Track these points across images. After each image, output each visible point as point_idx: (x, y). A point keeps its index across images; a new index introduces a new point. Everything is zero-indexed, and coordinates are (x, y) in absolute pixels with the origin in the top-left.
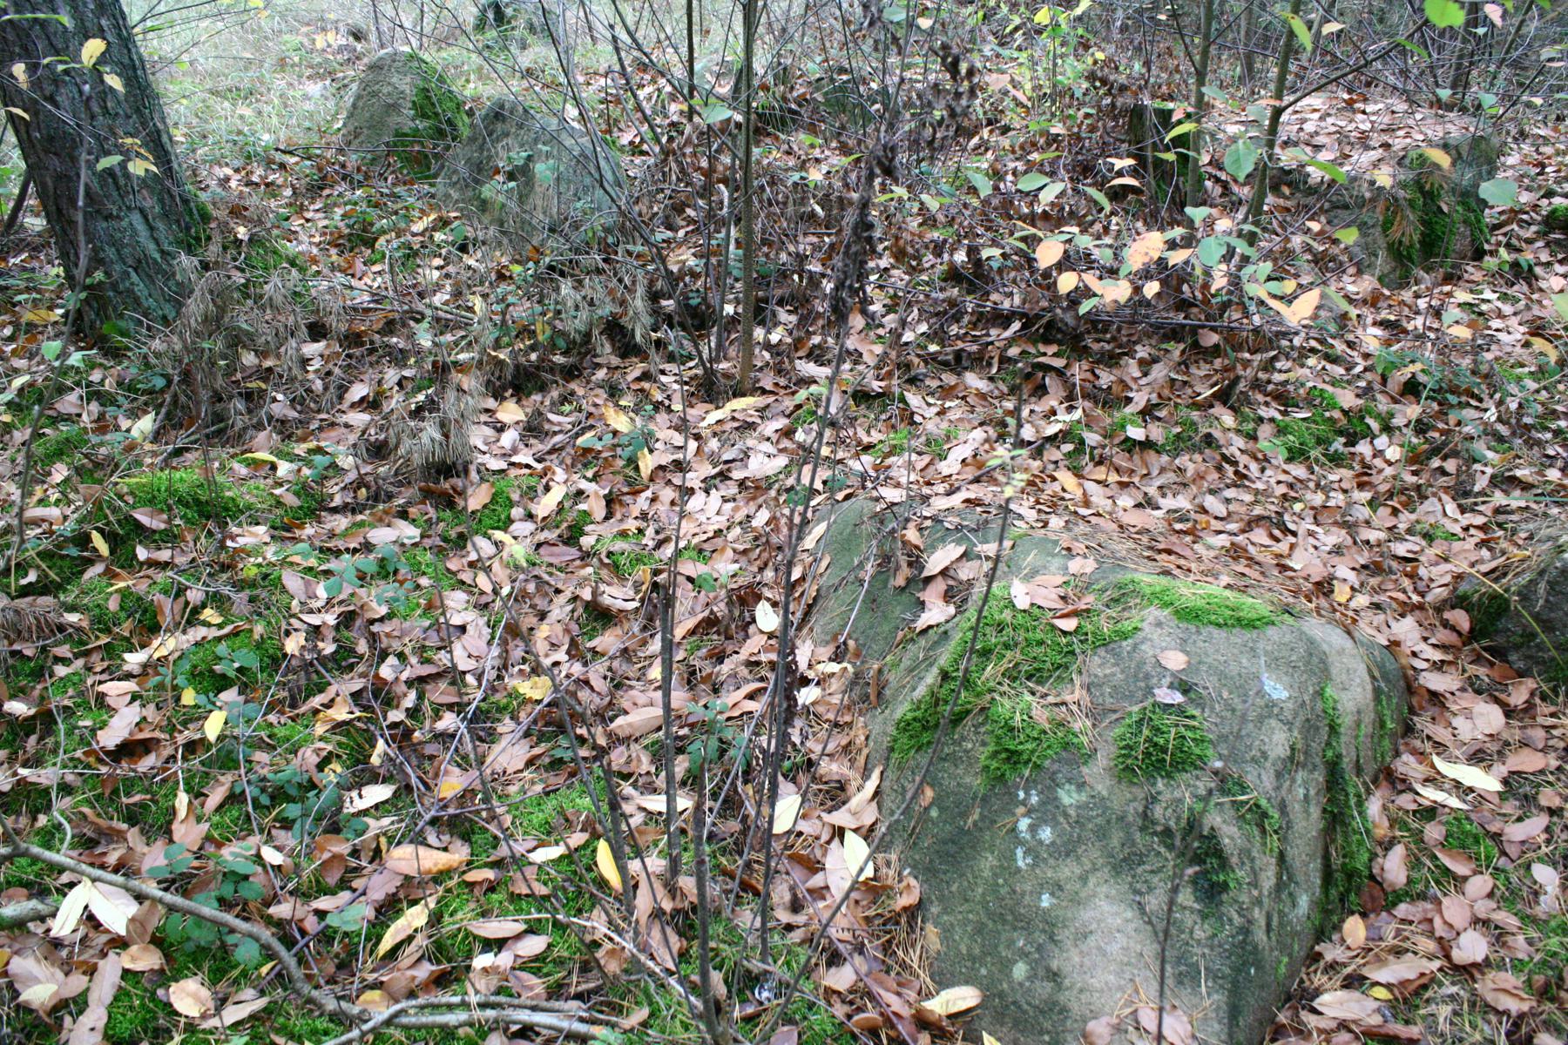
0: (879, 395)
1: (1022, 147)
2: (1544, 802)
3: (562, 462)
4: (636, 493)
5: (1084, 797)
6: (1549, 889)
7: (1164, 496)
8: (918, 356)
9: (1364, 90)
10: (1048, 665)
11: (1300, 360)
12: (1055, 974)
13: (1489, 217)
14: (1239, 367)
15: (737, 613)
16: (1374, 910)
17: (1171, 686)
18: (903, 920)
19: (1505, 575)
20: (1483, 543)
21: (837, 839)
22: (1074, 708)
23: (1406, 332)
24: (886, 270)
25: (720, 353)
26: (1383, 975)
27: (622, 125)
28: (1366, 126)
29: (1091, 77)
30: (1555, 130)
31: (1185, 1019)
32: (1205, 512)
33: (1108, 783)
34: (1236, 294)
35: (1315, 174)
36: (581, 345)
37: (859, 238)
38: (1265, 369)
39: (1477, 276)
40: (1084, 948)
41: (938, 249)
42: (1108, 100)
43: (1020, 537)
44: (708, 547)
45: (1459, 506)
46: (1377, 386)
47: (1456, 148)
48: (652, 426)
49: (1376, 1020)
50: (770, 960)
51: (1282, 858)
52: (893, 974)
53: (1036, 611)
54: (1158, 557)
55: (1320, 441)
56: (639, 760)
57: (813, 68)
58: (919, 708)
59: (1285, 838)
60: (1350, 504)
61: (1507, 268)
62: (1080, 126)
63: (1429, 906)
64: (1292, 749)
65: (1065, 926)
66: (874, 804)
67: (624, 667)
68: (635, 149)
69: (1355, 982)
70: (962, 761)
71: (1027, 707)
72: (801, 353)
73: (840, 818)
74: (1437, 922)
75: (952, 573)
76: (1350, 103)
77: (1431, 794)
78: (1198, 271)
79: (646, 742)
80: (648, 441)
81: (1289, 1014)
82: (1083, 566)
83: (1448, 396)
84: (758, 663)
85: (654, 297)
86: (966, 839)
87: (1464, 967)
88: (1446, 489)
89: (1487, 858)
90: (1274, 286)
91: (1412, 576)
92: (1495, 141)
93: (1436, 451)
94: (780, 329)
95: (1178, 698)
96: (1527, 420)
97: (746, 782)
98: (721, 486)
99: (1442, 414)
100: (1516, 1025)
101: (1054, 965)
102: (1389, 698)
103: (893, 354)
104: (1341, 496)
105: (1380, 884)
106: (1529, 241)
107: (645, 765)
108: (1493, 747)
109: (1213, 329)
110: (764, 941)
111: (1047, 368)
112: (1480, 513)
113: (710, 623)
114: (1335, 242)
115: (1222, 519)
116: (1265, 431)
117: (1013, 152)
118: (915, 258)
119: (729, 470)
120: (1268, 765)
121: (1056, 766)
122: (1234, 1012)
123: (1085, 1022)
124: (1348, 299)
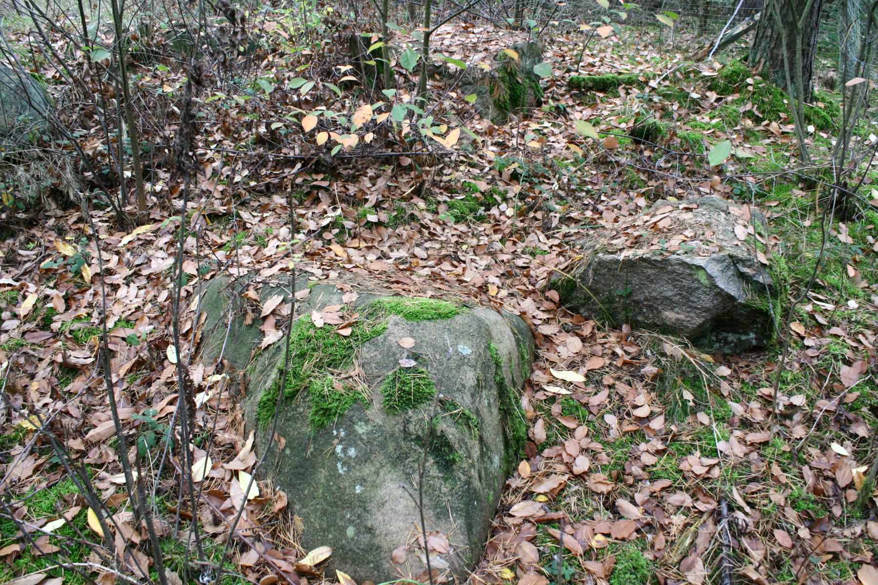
0: (224, 214)
1: (292, 64)
2: (605, 382)
3: (32, 279)
4: (83, 292)
5: (370, 428)
6: (613, 426)
7: (392, 251)
8: (244, 189)
9: (472, 21)
10: (339, 357)
11: (456, 168)
12: (370, 529)
13: (542, 84)
14: (424, 175)
15: (155, 355)
16: (532, 456)
17: (408, 357)
18: (280, 517)
19: (572, 269)
20: (560, 254)
21: (234, 478)
22: (357, 378)
23: (508, 147)
24: (220, 141)
25: (126, 201)
26: (542, 489)
27: (46, 66)
28: (475, 40)
29: (326, 22)
30: (567, 38)
31: (444, 537)
32: (415, 257)
33: (382, 417)
34: (418, 138)
35: (452, 67)
36: (36, 205)
37: (188, 124)
38: (438, 175)
39: (540, 115)
40: (383, 511)
41: (249, 126)
42: (337, 34)
43: (314, 286)
44: (132, 318)
45: (546, 236)
46: (497, 177)
47: (522, 49)
48: (88, 250)
49: (541, 513)
50: (205, 558)
51: (481, 439)
52: (279, 549)
53: (328, 327)
54: (392, 286)
55: (472, 210)
56: (107, 454)
57: (163, 25)
58: (269, 393)
59: (481, 428)
60: (492, 242)
61: (553, 110)
62: (323, 50)
63: (559, 448)
64: (478, 380)
65: (371, 501)
66: (253, 453)
67: (90, 399)
68: (57, 81)
69: (529, 496)
70: (297, 420)
71: (330, 382)
72: (175, 196)
73: (234, 465)
74: (564, 455)
75: (278, 312)
76: (466, 28)
77: (552, 389)
78: (394, 125)
79: (110, 442)
80: (87, 259)
81: (498, 520)
82: (351, 297)
83: (534, 179)
84: (172, 383)
85: (76, 170)
86: (308, 463)
87: (580, 475)
88: (538, 228)
89: (583, 417)
90: (435, 129)
91: (528, 276)
92: (540, 45)
93: (531, 208)
94: (161, 183)
95: (413, 363)
96: (573, 187)
97: (174, 455)
98: (136, 280)
99: (532, 189)
100: (607, 498)
101: (369, 524)
102: (524, 343)
103: (230, 190)
104: (486, 238)
105: (533, 441)
106: (562, 95)
107: (112, 456)
108: (578, 359)
109: (407, 156)
110: (200, 548)
111: (319, 188)
112: (556, 238)
113: (139, 364)
114: (467, 103)
115: (425, 259)
116: (442, 208)
117: (287, 66)
118: (236, 133)
119: (140, 270)
120: (466, 391)
121: (351, 413)
122: (469, 527)
123: (391, 551)
124: (476, 132)
